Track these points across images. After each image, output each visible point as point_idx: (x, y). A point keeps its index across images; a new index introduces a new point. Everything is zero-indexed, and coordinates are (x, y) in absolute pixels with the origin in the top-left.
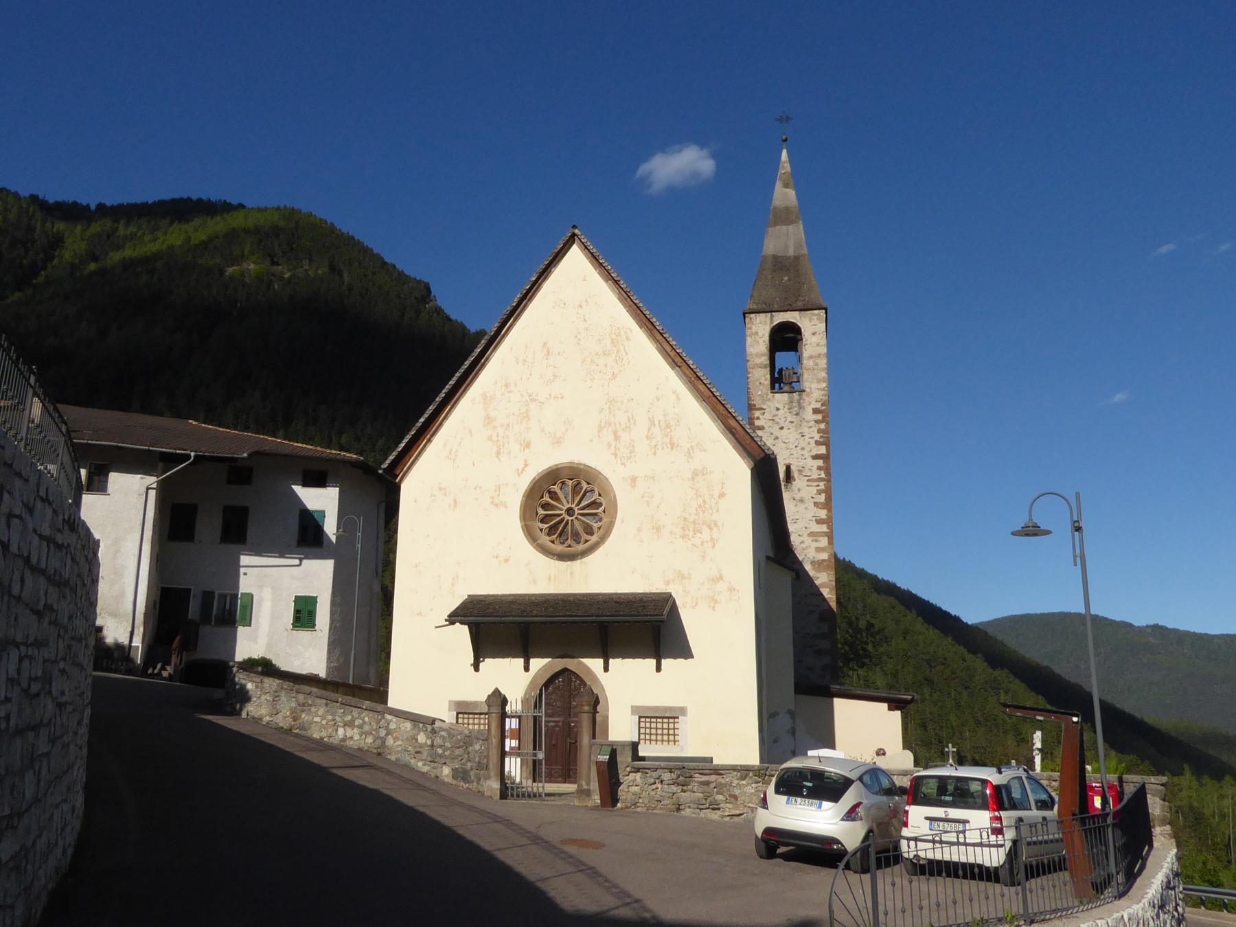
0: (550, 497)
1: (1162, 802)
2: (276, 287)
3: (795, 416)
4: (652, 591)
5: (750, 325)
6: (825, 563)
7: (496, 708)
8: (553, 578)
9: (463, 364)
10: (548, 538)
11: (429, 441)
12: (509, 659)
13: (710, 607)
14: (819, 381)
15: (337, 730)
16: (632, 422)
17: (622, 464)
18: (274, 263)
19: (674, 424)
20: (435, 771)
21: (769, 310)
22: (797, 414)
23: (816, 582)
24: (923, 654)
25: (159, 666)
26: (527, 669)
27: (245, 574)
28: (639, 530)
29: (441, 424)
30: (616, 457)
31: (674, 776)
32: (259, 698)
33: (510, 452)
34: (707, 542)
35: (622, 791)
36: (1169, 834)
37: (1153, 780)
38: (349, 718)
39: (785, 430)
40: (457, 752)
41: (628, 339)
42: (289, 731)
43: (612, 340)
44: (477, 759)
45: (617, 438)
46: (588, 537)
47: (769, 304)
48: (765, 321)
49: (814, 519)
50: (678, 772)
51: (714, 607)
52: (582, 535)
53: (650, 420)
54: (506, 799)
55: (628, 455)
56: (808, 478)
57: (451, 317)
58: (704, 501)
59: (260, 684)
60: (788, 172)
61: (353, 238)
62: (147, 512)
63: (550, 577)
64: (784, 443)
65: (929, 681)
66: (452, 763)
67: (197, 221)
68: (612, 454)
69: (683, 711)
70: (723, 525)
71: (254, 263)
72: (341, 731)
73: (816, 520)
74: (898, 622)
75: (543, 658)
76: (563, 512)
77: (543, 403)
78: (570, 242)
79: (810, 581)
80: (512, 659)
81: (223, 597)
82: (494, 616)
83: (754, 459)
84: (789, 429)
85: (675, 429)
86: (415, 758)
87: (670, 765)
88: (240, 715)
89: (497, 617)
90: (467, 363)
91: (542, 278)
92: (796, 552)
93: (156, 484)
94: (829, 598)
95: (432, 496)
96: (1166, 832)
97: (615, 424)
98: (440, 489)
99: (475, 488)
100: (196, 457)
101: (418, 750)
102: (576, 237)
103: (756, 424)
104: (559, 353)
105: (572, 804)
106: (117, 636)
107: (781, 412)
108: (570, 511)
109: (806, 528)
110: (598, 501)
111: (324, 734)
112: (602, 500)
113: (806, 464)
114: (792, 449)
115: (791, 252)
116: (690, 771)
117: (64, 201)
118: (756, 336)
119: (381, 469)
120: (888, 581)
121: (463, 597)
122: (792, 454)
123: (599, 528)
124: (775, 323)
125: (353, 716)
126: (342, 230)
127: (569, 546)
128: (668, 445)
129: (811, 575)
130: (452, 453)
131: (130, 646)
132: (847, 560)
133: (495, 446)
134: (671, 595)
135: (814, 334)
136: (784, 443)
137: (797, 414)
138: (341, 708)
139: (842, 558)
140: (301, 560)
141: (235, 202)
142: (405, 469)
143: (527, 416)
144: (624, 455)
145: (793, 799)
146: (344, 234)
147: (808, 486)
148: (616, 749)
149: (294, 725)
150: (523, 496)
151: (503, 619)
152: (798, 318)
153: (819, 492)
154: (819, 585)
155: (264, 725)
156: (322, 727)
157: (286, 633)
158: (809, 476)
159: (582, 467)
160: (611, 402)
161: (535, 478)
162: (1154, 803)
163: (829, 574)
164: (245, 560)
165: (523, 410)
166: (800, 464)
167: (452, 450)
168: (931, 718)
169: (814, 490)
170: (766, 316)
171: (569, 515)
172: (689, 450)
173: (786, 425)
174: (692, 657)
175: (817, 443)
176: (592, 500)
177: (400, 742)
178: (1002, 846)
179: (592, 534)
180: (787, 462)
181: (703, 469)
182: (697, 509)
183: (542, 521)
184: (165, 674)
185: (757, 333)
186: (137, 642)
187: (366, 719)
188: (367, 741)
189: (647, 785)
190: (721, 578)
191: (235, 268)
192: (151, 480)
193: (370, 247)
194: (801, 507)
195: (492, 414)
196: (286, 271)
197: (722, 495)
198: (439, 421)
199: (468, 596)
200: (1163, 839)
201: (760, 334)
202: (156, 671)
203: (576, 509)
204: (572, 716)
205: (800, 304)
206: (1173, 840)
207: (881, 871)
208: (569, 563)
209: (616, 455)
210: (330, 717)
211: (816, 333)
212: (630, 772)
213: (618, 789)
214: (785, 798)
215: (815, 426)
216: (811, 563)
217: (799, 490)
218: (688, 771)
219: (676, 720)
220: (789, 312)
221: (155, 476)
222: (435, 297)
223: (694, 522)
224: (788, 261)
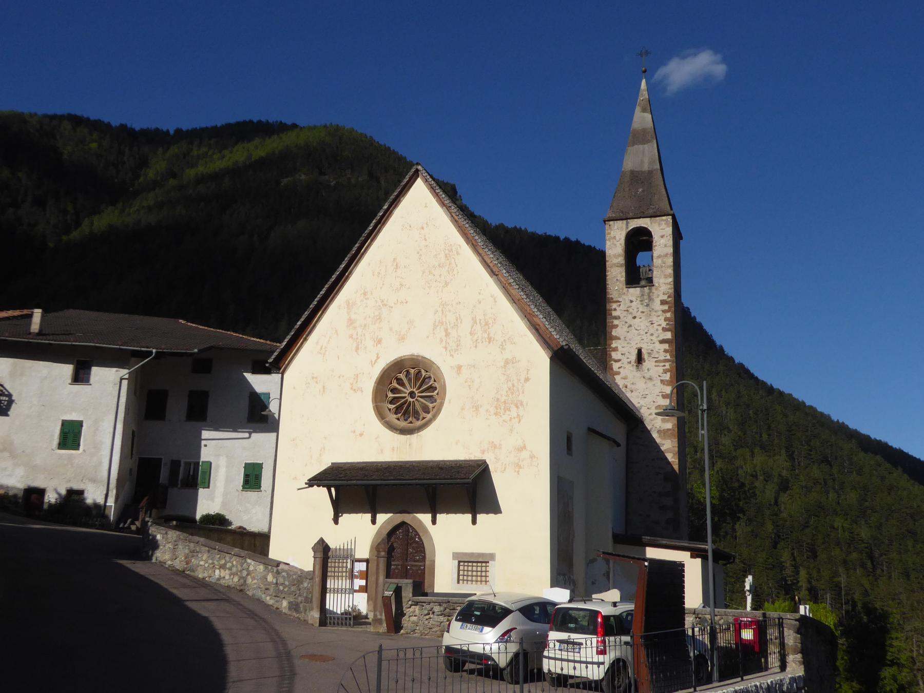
0: (397, 383)
1: (795, 634)
2: (324, 194)
3: (646, 307)
4: (471, 459)
5: (609, 231)
6: (669, 432)
7: (319, 553)
8: (396, 449)
9: (331, 277)
10: (395, 416)
11: (306, 339)
12: (361, 514)
13: (515, 471)
14: (666, 277)
15: (215, 572)
16: (459, 321)
17: (451, 356)
18: (322, 173)
19: (491, 322)
20: (277, 604)
21: (625, 218)
22: (647, 305)
23: (661, 448)
24: (907, 508)
25: (129, 521)
26: (374, 522)
27: (206, 446)
28: (463, 409)
29: (314, 326)
30: (446, 350)
31: (442, 609)
32: (165, 546)
33: (366, 348)
34: (514, 418)
35: (405, 621)
36: (799, 662)
37: (788, 616)
38: (223, 562)
39: (637, 320)
40: (293, 588)
41: (458, 254)
42: (181, 573)
43: (446, 255)
44: (305, 595)
45: (447, 335)
46: (424, 415)
47: (626, 212)
48: (622, 227)
49: (661, 394)
50: (445, 605)
51: (518, 472)
52: (421, 413)
53: (473, 319)
54: (325, 626)
55: (456, 348)
56: (656, 359)
57: (475, 214)
58: (513, 385)
59: (165, 535)
60: (646, 99)
61: (389, 148)
62: (120, 398)
63: (393, 448)
64: (636, 330)
65: (913, 533)
66: (289, 597)
67: (257, 141)
68: (443, 347)
69: (492, 556)
70: (527, 404)
71: (304, 174)
72: (217, 572)
73: (662, 395)
74: (883, 478)
75: (386, 513)
76: (407, 395)
77: (392, 307)
78: (414, 178)
79: (656, 447)
80: (363, 514)
81: (188, 464)
82: (342, 480)
83: (553, 350)
84: (640, 318)
85: (492, 326)
86: (265, 593)
87: (439, 600)
88: (151, 559)
89: (345, 480)
90: (334, 277)
91: (393, 206)
92: (645, 423)
93: (128, 375)
94: (673, 462)
95: (306, 384)
96: (797, 660)
97: (446, 323)
98: (313, 378)
99: (339, 377)
100: (157, 353)
101: (267, 587)
102: (419, 172)
103: (613, 315)
104: (405, 267)
105: (369, 630)
106: (95, 497)
107: (634, 303)
108: (412, 394)
109: (654, 402)
110: (433, 385)
111: (206, 575)
112: (436, 385)
113: (654, 347)
114: (643, 335)
115: (646, 168)
116: (454, 605)
117: (148, 128)
118: (614, 240)
119: (267, 363)
120: (880, 441)
121: (328, 464)
122: (643, 339)
123: (434, 408)
124: (630, 228)
125: (226, 560)
126: (380, 143)
127: (411, 422)
128: (487, 339)
129: (658, 443)
130: (323, 349)
131: (105, 505)
132: (841, 421)
133: (355, 342)
134: (485, 462)
135: (662, 237)
136: (636, 330)
137: (647, 305)
138: (218, 554)
139: (836, 420)
140: (250, 433)
141: (289, 122)
142: (286, 363)
143: (379, 318)
144: (453, 348)
145: (465, 624)
146: (381, 145)
147: (655, 366)
148: (401, 587)
149: (186, 568)
150: (375, 383)
151: (349, 482)
152: (649, 223)
153: (665, 372)
154: (665, 450)
155: (166, 568)
156: (205, 569)
157: (237, 493)
158: (657, 358)
159: (420, 358)
160: (443, 305)
161: (384, 368)
162: (789, 635)
163: (672, 441)
164: (205, 434)
165: (377, 313)
166: (649, 347)
167: (322, 346)
168: (914, 568)
169: (661, 369)
170: (623, 223)
171: (412, 397)
172: (502, 343)
173: (638, 315)
174: (500, 512)
175: (664, 330)
176: (429, 385)
177: (255, 581)
178: (603, 663)
179: (428, 412)
180: (639, 346)
181: (513, 358)
182: (507, 392)
183: (391, 403)
184: (133, 528)
185: (615, 238)
186: (111, 502)
187: (234, 563)
188: (234, 579)
189: (423, 616)
190: (524, 447)
191: (289, 179)
192: (124, 372)
193: (404, 155)
194: (650, 384)
195: (353, 317)
196: (331, 180)
197: (527, 380)
198: (313, 324)
199: (332, 463)
200: (794, 665)
201: (617, 238)
202: (126, 526)
203: (416, 392)
204: (408, 561)
205: (651, 211)
206: (803, 666)
207: (527, 684)
208: (408, 436)
209: (446, 348)
210: (210, 561)
211: (664, 235)
212: (411, 605)
213: (402, 618)
214: (460, 623)
215: (663, 315)
216: (658, 432)
217: (648, 370)
218: (452, 604)
219: (487, 564)
220: (641, 219)
221: (127, 369)
222: (460, 196)
223: (505, 402)
224: (643, 175)
